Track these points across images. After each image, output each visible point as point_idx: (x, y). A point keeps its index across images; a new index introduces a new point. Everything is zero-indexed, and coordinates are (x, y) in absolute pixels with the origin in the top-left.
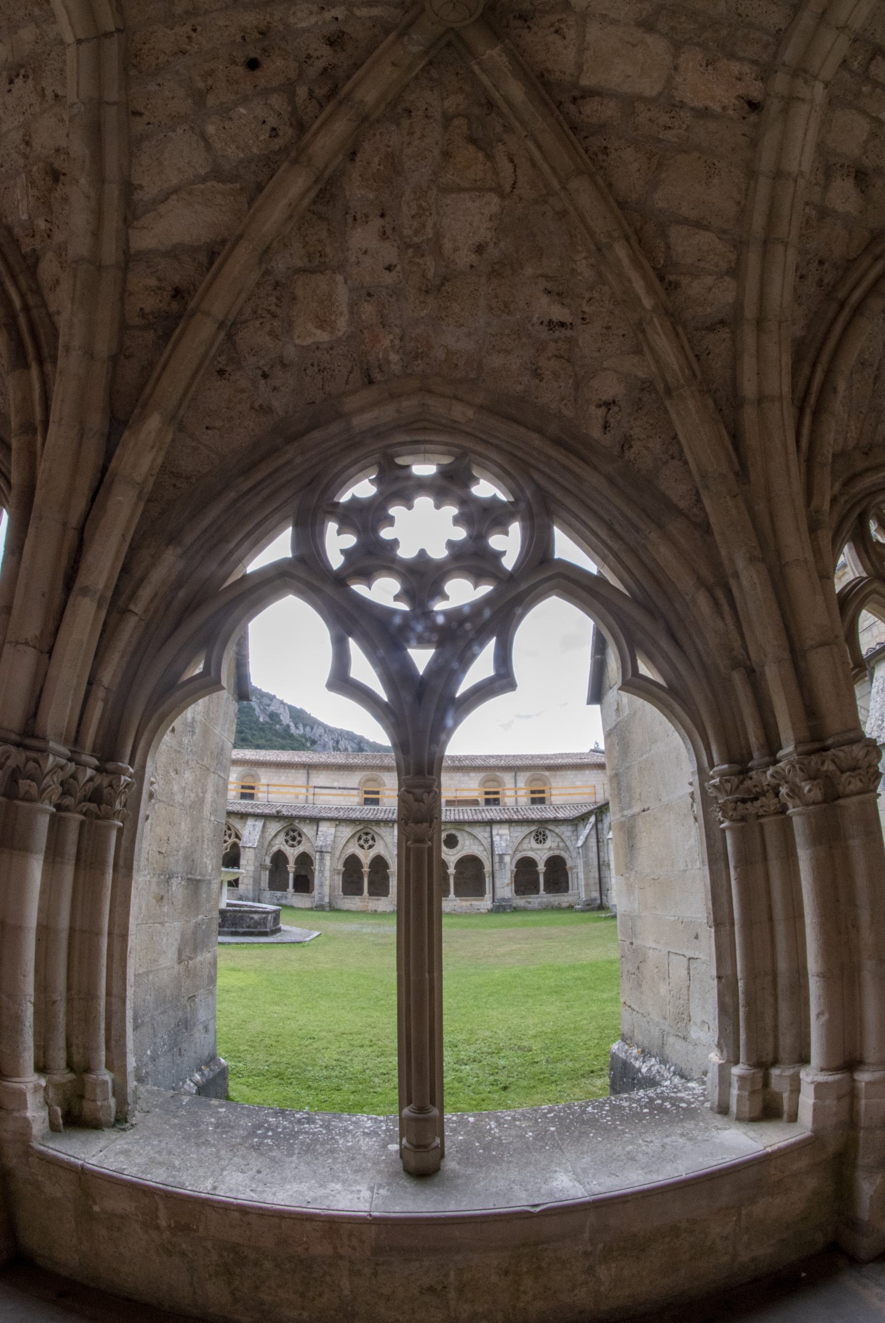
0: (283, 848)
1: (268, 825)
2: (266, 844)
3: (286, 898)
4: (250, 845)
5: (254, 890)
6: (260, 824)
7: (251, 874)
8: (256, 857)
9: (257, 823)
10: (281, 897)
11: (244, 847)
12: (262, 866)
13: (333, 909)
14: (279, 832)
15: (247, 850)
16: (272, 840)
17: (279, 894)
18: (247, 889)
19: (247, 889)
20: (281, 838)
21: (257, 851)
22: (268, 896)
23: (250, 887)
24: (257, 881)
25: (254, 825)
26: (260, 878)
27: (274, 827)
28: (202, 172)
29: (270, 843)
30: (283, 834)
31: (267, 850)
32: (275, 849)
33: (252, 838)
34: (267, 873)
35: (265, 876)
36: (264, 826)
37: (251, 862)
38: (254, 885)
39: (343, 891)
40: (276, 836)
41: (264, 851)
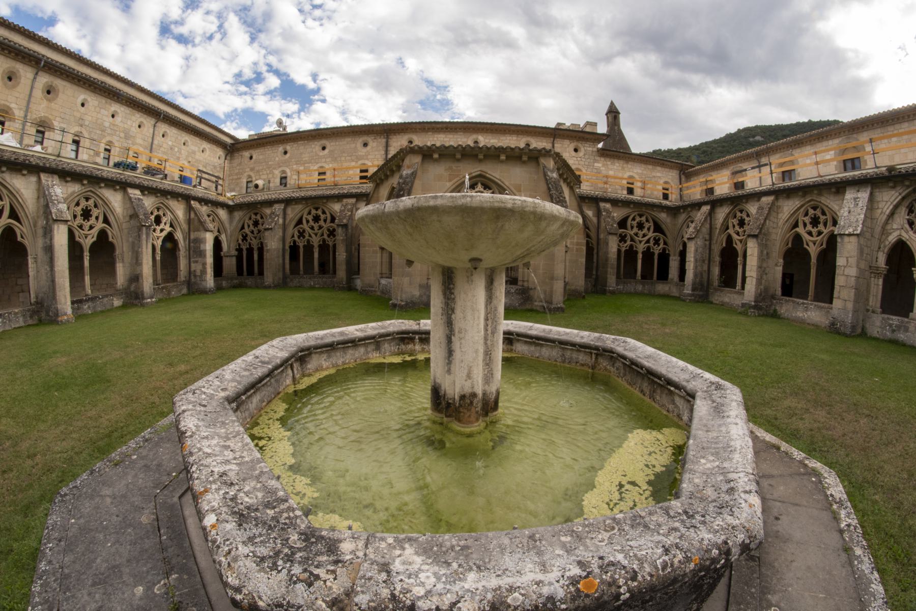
0: (905, 236)
1: (781, 202)
2: (878, 229)
3: (907, 330)
4: (851, 230)
5: (855, 311)
6: (864, 195)
7: (852, 281)
8: (861, 251)
9: (859, 195)
10: (899, 327)
11: (841, 235)
12: (873, 270)
13: (860, 333)
14: (896, 207)
15: (846, 239)
16: (886, 222)
17: (895, 320)
18: (845, 309)
19: (845, 309)
20: (902, 217)
21: (862, 241)
22: (878, 324)
23: (850, 306)
24: (861, 295)
25: (855, 199)
26: (868, 291)
27: (888, 198)
28: (435, 217)
29: (883, 228)
30: (903, 211)
31: (881, 241)
32: (892, 238)
33: (853, 219)
34: (881, 282)
35: (877, 285)
36: (871, 199)
37: (853, 261)
38: (856, 301)
39: (881, 307)
40: (892, 214)
41: (875, 243)
